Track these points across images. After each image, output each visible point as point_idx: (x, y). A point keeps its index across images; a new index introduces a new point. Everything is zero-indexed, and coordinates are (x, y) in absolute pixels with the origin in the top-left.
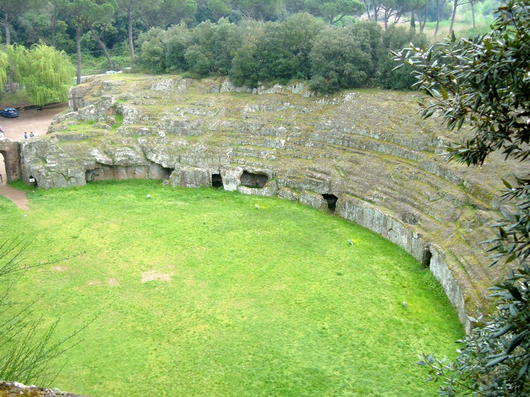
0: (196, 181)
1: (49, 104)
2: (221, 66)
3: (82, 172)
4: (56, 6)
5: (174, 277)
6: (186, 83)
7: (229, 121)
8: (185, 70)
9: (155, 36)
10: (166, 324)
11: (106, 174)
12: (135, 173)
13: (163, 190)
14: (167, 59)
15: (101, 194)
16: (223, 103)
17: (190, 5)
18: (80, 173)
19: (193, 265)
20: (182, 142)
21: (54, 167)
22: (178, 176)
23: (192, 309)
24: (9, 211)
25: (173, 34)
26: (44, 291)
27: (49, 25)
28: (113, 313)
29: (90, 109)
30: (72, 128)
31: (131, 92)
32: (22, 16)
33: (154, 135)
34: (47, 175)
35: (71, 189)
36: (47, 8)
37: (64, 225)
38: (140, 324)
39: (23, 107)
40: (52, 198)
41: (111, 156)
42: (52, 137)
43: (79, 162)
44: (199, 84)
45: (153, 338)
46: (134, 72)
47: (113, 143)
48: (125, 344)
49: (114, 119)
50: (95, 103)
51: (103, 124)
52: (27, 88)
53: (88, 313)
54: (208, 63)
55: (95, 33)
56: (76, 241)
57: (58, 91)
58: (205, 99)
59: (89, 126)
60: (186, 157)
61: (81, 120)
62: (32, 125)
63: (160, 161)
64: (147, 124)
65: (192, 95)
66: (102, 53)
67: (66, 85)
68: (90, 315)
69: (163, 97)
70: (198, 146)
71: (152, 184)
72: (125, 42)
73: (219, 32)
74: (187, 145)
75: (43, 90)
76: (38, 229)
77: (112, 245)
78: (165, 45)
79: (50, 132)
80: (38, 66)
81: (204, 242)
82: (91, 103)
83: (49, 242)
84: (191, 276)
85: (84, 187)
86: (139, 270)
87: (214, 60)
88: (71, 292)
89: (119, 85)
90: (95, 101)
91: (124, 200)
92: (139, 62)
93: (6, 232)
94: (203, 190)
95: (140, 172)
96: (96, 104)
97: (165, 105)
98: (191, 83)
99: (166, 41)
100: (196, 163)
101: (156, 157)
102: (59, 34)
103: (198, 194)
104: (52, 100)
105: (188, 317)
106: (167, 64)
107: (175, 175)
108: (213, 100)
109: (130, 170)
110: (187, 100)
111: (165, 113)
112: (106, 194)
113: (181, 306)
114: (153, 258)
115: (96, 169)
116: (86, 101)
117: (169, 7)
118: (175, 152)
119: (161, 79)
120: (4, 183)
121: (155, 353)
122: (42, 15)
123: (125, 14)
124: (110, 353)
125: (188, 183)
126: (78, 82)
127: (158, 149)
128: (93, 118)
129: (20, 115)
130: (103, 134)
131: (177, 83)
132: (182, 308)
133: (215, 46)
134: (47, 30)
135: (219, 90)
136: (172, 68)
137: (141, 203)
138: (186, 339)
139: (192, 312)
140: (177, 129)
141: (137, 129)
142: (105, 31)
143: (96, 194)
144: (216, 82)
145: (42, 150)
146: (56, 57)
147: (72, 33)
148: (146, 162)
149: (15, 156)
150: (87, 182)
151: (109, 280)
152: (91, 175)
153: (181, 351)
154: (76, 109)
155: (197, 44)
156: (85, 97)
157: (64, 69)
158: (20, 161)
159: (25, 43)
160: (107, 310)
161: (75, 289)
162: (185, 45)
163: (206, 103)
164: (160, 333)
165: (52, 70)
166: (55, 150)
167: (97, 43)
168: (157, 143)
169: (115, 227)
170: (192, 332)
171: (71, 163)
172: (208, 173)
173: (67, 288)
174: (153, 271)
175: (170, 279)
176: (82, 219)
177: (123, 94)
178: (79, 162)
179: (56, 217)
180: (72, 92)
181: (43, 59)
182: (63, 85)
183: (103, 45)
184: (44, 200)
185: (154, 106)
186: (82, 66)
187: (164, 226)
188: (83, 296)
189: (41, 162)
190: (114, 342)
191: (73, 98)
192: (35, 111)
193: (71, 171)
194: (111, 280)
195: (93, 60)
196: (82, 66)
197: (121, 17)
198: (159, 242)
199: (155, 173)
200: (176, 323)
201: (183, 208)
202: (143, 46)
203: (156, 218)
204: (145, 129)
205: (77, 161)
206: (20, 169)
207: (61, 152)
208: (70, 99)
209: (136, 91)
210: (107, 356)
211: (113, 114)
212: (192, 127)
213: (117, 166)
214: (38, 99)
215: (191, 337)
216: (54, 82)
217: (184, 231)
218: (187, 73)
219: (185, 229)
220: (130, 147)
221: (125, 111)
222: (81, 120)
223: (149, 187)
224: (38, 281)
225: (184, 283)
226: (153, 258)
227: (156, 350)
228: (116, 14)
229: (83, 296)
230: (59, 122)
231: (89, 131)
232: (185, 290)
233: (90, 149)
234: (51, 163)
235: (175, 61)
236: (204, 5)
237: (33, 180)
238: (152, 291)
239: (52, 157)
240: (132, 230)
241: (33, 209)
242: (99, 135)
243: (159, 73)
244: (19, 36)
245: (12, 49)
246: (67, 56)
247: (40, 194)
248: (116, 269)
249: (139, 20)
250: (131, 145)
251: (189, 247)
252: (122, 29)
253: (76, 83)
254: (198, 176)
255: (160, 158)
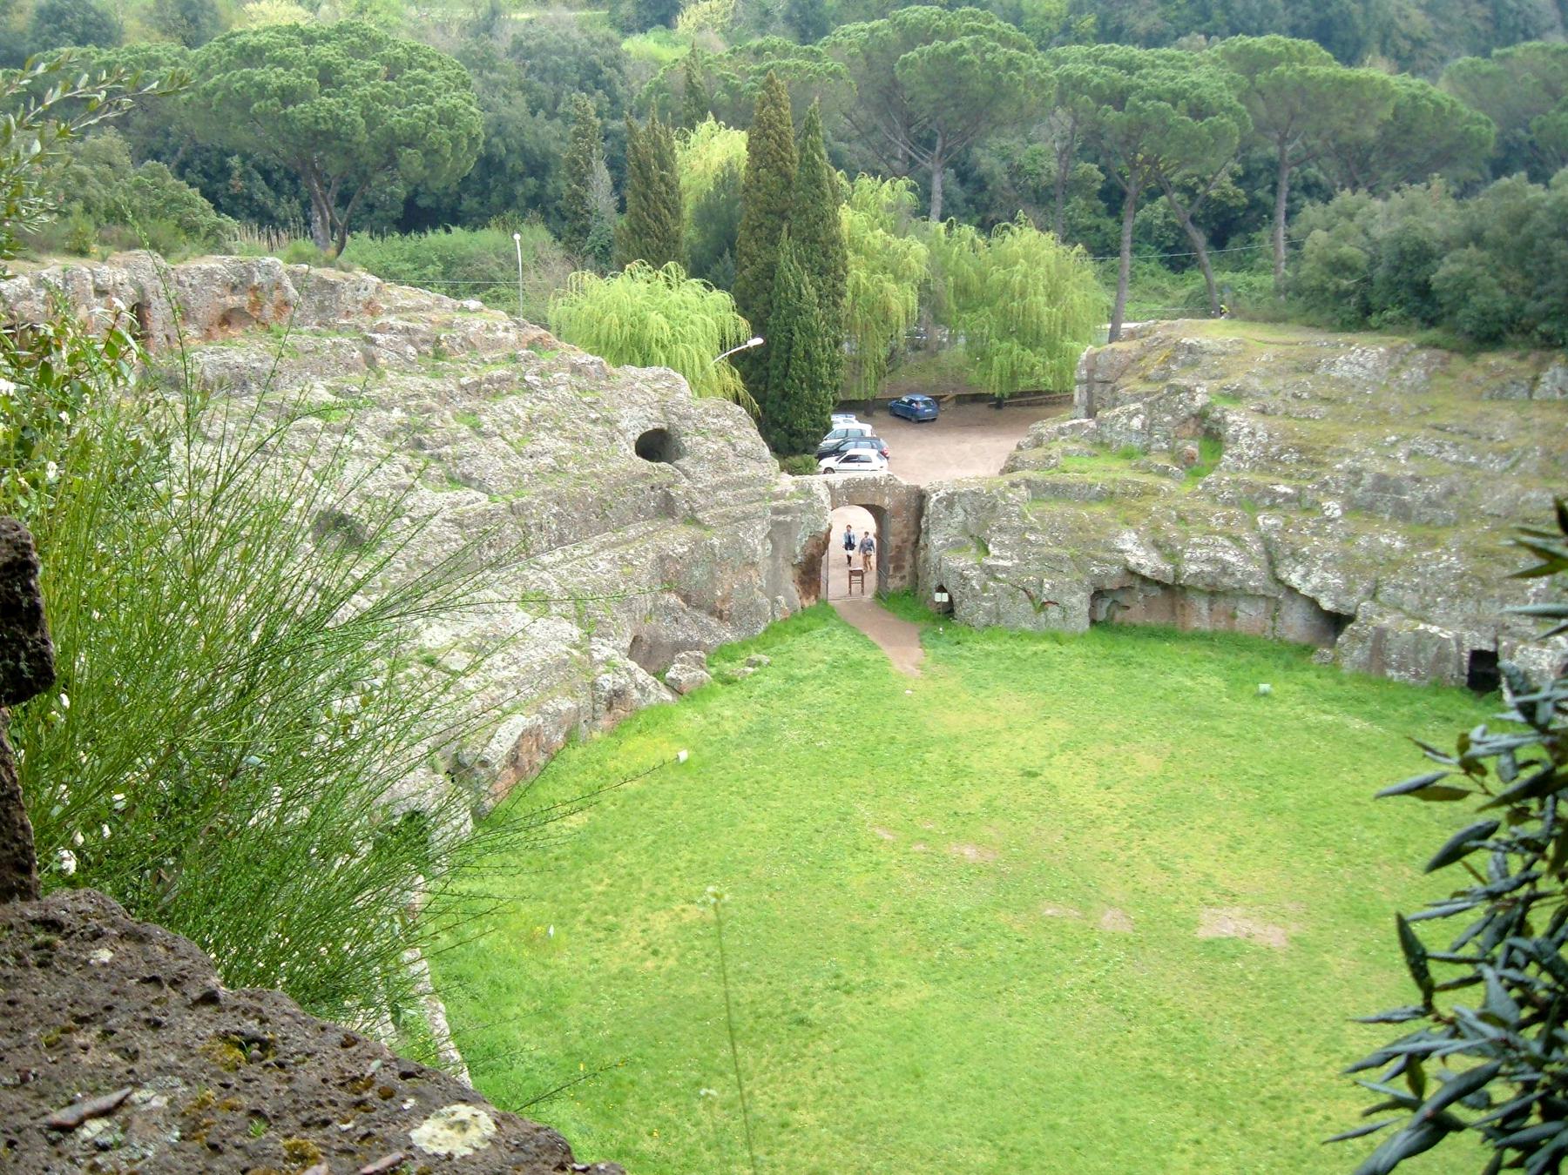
0: (1417, 663)
1: (1023, 394)
2: (1547, 316)
3: (1081, 594)
4: (1076, 122)
5: (1297, 940)
6: (1428, 363)
7: (1551, 490)
8: (1431, 323)
9: (1351, 216)
10: (1245, 1074)
11: (1148, 609)
12: (1234, 617)
13: (1310, 676)
14: (1377, 287)
15: (1127, 662)
16: (1536, 434)
17: (1474, 128)
18: (1075, 593)
19: (1364, 916)
20: (1393, 540)
21: (1006, 570)
22: (1363, 640)
23: (1333, 1046)
24: (867, 672)
25: (1402, 212)
26: (919, 906)
27: (1054, 173)
28: (1095, 1009)
29: (1131, 416)
30: (1073, 463)
31: (1255, 375)
32: (984, 148)
33: (1308, 509)
34: (985, 588)
35: (1045, 638)
36: (1051, 127)
37: (1006, 736)
38: (1168, 1057)
39: (952, 394)
40: (988, 655)
41: (1173, 556)
42: (1014, 485)
43: (1079, 563)
44: (1470, 370)
45: (1197, 1107)
46: (1275, 319)
47: (1181, 518)
48: (1113, 1104)
49: (1196, 450)
50: (1147, 400)
51: (1162, 461)
52: (970, 343)
53: (1026, 993)
54: (1504, 305)
55: (1181, 202)
56: (1033, 784)
57: (1051, 358)
58: (1479, 418)
59: (1123, 463)
60: (1396, 587)
61: (1101, 445)
62: (966, 447)
63: (1315, 589)
64: (1289, 476)
65: (1440, 400)
66: (1195, 261)
67: (1076, 345)
68: (1030, 999)
69: (1350, 400)
70: (1439, 557)
71: (1279, 654)
72: (1265, 233)
73: (1551, 211)
74: (1404, 551)
75: (1010, 352)
76: (934, 734)
77: (1132, 812)
78: (1376, 243)
79: (1009, 469)
80: (1006, 284)
81: (1409, 851)
82: (1137, 397)
83: (958, 773)
84: (1351, 948)
85: (1083, 636)
86: (1196, 900)
87: (1522, 299)
88: (991, 924)
89: (1224, 354)
90: (1148, 394)
91: (1191, 690)
92: (1295, 290)
93: (848, 727)
94: (1437, 694)
95: (1249, 615)
96: (1151, 404)
97: (1352, 423)
98: (1442, 363)
99: (1379, 232)
100: (1425, 608)
101: (1305, 577)
102: (1079, 201)
103: (1419, 706)
104: (1033, 382)
105: (1316, 1069)
106: (1375, 300)
107: (1354, 636)
108: (1504, 421)
109: (1221, 604)
110: (1424, 413)
111: (1349, 446)
112: (1141, 665)
113: (1300, 1031)
114: (1245, 874)
115: (1122, 588)
116: (1122, 391)
117: (1408, 131)
118: (1365, 566)
119: (1350, 345)
120: (869, 596)
121: (1193, 1152)
122: (1037, 146)
123: (1273, 150)
124: (1064, 1121)
125: (1390, 666)
126: (1114, 336)
127: (1314, 551)
128: (1137, 443)
129: (941, 416)
130: (1156, 492)
131: (1398, 360)
132: (1304, 1036)
133: (1533, 256)
134: (1046, 188)
135: (1531, 393)
136: (1389, 314)
137: (1238, 707)
138: (1297, 1133)
139: (1333, 1056)
140: (1377, 499)
141: (1258, 487)
142: (1208, 197)
143: (1111, 661)
144: (1524, 365)
145: (982, 513)
146: (1057, 262)
147: (1113, 198)
148: (1272, 586)
149: (905, 526)
150: (1093, 622)
151: (1104, 914)
152: (1106, 604)
153: (1273, 1165)
154: (1091, 413)
155: (1477, 245)
156: (1122, 381)
157: (1077, 298)
158: (917, 541)
159: (984, 220)
160: (1081, 998)
161: (1003, 917)
162: (1437, 247)
163: (1482, 429)
164: (1223, 1096)
165: (1042, 299)
166: (1016, 522)
167: (1182, 232)
168: (1313, 534)
169: (1148, 763)
170: (1317, 1117)
171: (1054, 564)
172: (1459, 644)
173: (982, 911)
174: (1238, 911)
175: (1283, 944)
176: (1062, 726)
177: (1232, 380)
178: (1079, 563)
179: (989, 709)
180: (1086, 362)
181: (1022, 266)
182: (1068, 343)
183: (1199, 238)
184: (966, 658)
185: (1318, 424)
186: (1128, 293)
187: (1294, 782)
188: (1020, 941)
189: (973, 550)
190: (1082, 1091)
191: (1087, 381)
192: (981, 408)
193: (1053, 586)
194: (1110, 913)
195: (1165, 280)
196: (1128, 293)
197: (1261, 159)
198: (1271, 828)
199: (1295, 623)
200: (1277, 1079)
201: (1362, 740)
202: (1308, 245)
203: (1275, 755)
204: (1281, 489)
205: (1072, 558)
206: (915, 565)
207: (1033, 530)
208: (1078, 382)
209: (1271, 373)
210: (1053, 1127)
211: (1194, 437)
212: (1428, 498)
213: (1184, 588)
214: (995, 377)
215: (1314, 1131)
216: (1045, 331)
217: (1354, 809)
218: (1434, 334)
219: (1357, 804)
220: (1230, 537)
221: (1231, 430)
222: (1102, 444)
223: (1270, 662)
224: (907, 876)
225: (1322, 965)
226: (1245, 874)
227: (1198, 1142)
228: (1246, 147)
229: (1020, 941)
230: (1038, 442)
231: (1118, 476)
232: (1322, 984)
233: (1112, 530)
234: (1001, 557)
235: (1403, 295)
236: (1521, 132)
237: (944, 598)
238: (1223, 967)
239: (1006, 539)
240: (1198, 779)
241: (933, 678)
242: (1145, 492)
243: (1346, 326)
244: (968, 201)
245: (942, 235)
246: (1089, 261)
247: (956, 639)
248: (1131, 885)
249: (1313, 171)
250: (1235, 533)
251: (1359, 861)
252: (1259, 193)
253: (1106, 338)
254: (1424, 649)
255: (1315, 580)
